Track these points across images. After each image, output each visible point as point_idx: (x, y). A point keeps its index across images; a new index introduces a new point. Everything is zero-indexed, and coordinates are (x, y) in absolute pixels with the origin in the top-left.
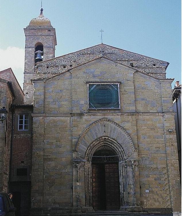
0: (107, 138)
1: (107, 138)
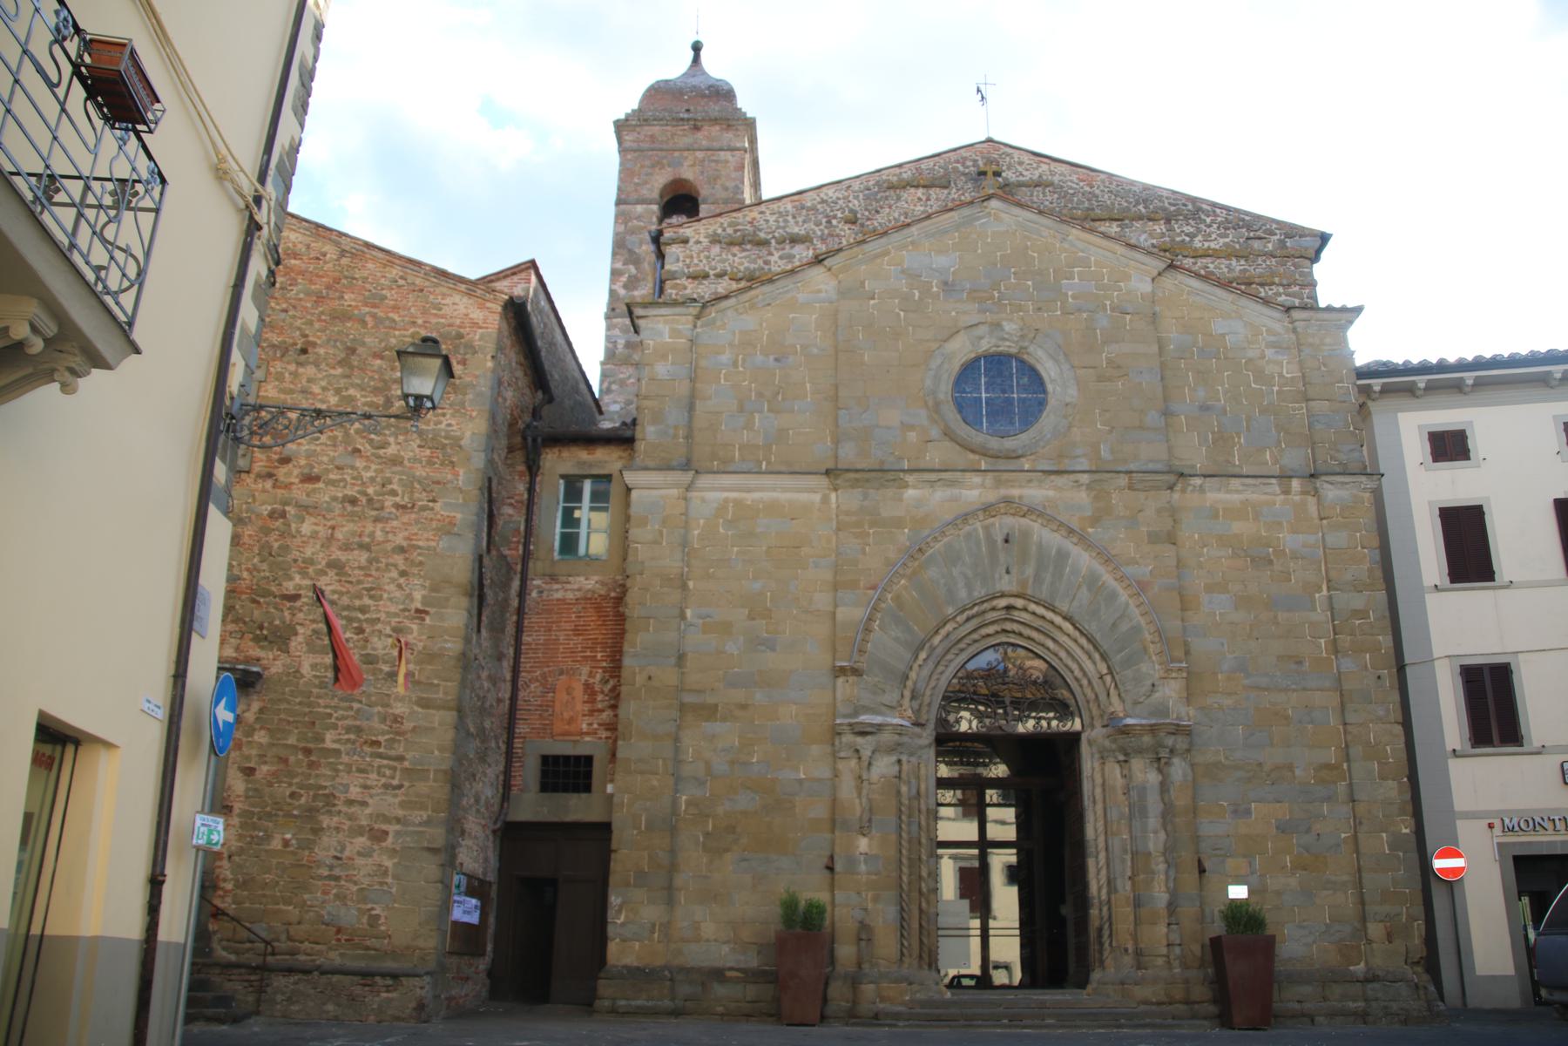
0: (1019, 603)
1: (1019, 603)
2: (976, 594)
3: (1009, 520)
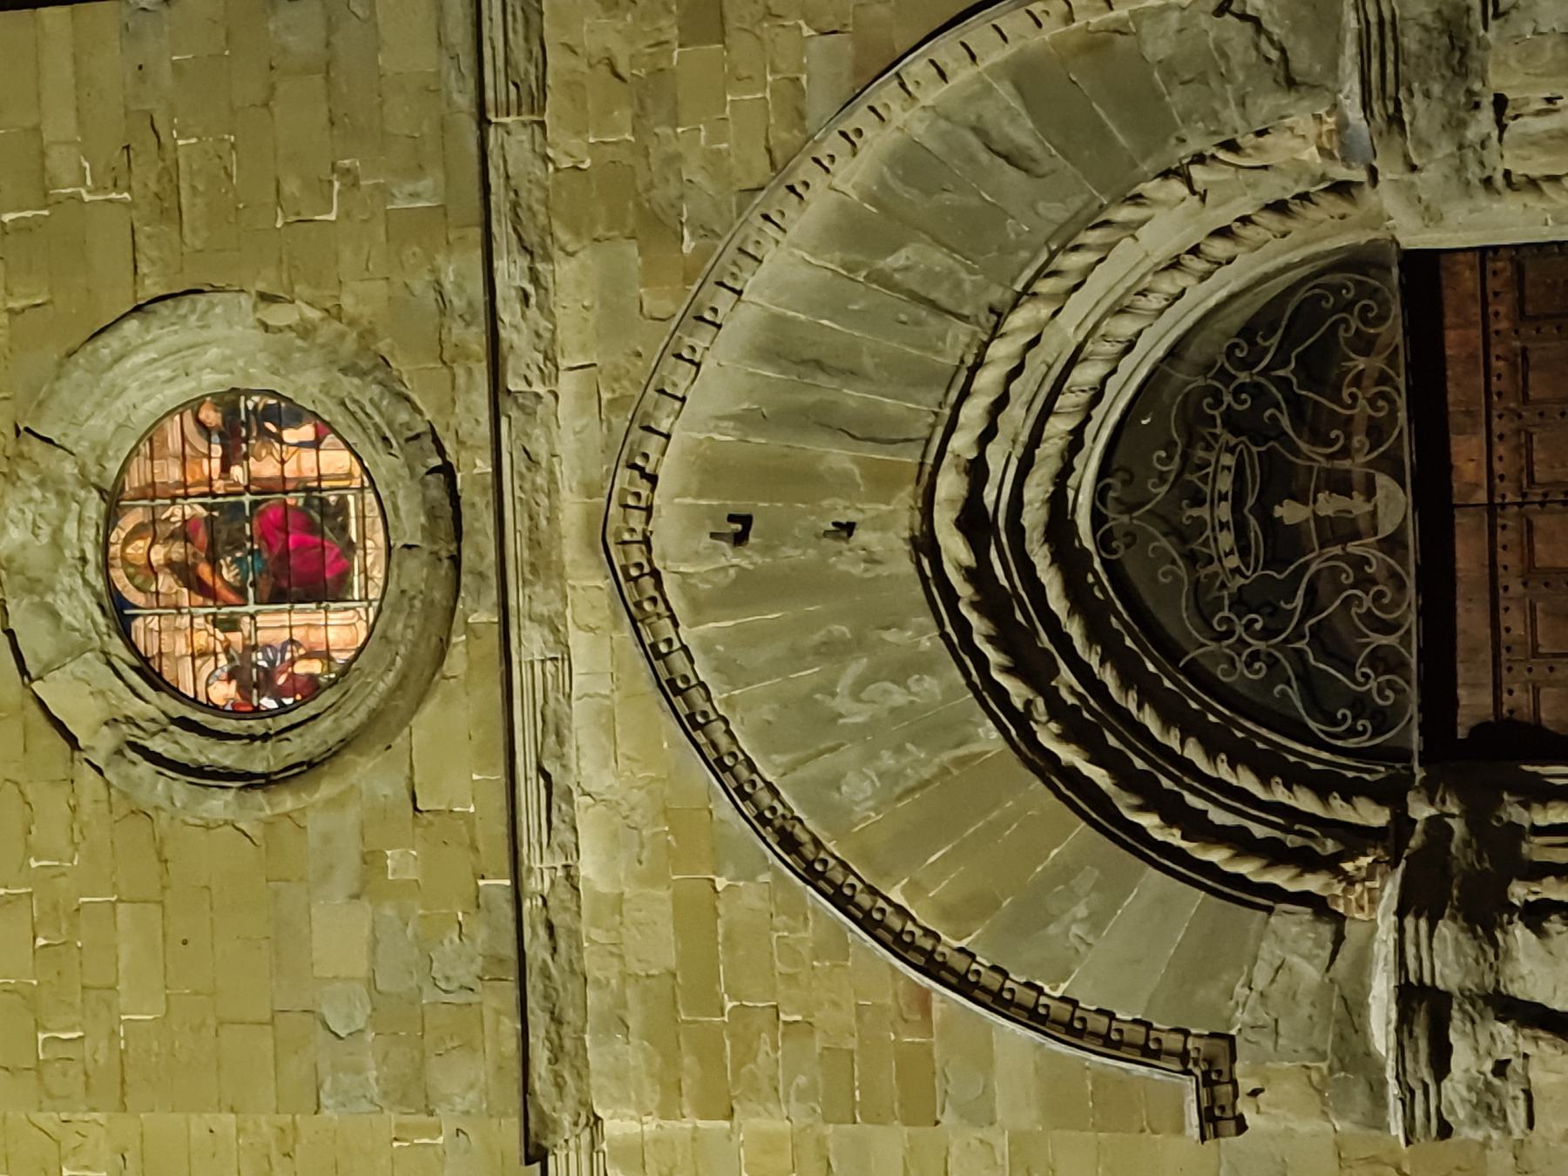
1: (950, 486)
2: (929, 642)
3: (667, 530)
